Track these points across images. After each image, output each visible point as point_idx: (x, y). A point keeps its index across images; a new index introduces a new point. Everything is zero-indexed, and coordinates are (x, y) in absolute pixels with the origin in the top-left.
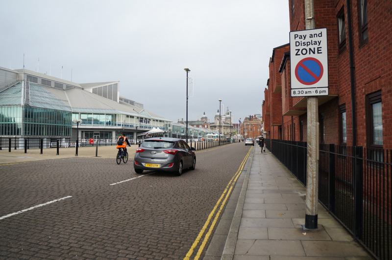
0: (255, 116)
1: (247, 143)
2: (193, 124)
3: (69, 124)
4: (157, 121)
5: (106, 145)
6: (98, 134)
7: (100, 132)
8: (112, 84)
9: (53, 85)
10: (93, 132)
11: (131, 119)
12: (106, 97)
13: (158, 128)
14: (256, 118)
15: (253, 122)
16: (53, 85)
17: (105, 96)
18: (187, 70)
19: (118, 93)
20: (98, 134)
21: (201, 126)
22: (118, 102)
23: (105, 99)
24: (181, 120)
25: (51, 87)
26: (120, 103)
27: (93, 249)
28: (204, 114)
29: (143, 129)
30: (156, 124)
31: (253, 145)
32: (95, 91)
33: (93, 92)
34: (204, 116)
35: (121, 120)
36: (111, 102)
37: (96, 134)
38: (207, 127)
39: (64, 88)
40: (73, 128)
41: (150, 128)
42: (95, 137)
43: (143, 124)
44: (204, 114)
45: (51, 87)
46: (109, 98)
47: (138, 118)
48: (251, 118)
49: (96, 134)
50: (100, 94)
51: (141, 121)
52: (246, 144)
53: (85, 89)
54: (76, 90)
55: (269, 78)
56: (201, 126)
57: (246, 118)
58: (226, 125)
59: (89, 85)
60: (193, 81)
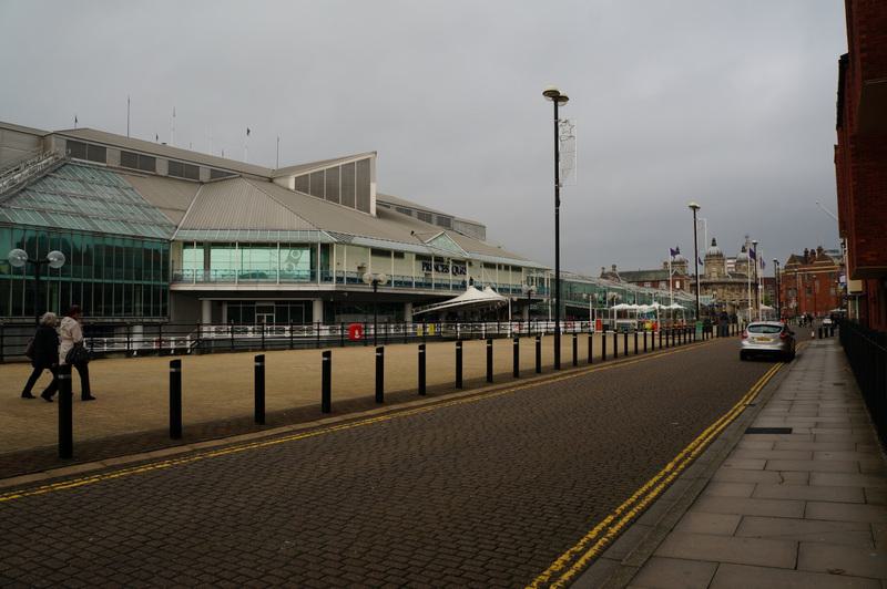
0: (820, 250)
1: (747, 345)
2: (641, 279)
3: (157, 278)
4: (507, 267)
5: (129, 354)
6: (270, 310)
7: (276, 302)
8: (355, 160)
9: (162, 168)
10: (254, 302)
11: (399, 261)
12: (337, 201)
13: (489, 290)
14: (823, 257)
15: (816, 269)
16: (162, 168)
17: (333, 197)
18: (557, 97)
19: (373, 187)
20: (270, 310)
21: (663, 284)
22: (373, 212)
23: (332, 206)
24: (609, 269)
25: (202, 183)
26: (380, 214)
27: (430, 581)
28: (714, 244)
29: (433, 292)
30: (485, 276)
31: (786, 356)
32: (302, 185)
33: (298, 187)
34: (714, 250)
35: (343, 264)
36: (352, 213)
37: (262, 310)
38: (682, 287)
39: (204, 175)
40: (172, 291)
41: (463, 287)
42: (260, 318)
43: (435, 276)
44: (714, 244)
45: (202, 183)
46: (329, 198)
47: (419, 257)
48: (807, 258)
49: (262, 310)
50: (317, 193)
51: (427, 266)
52: (749, 355)
53: (277, 181)
54: (244, 187)
55: (845, 50)
56: (663, 284)
57: (793, 259)
58: (736, 280)
59: (286, 172)
60: (575, 132)
